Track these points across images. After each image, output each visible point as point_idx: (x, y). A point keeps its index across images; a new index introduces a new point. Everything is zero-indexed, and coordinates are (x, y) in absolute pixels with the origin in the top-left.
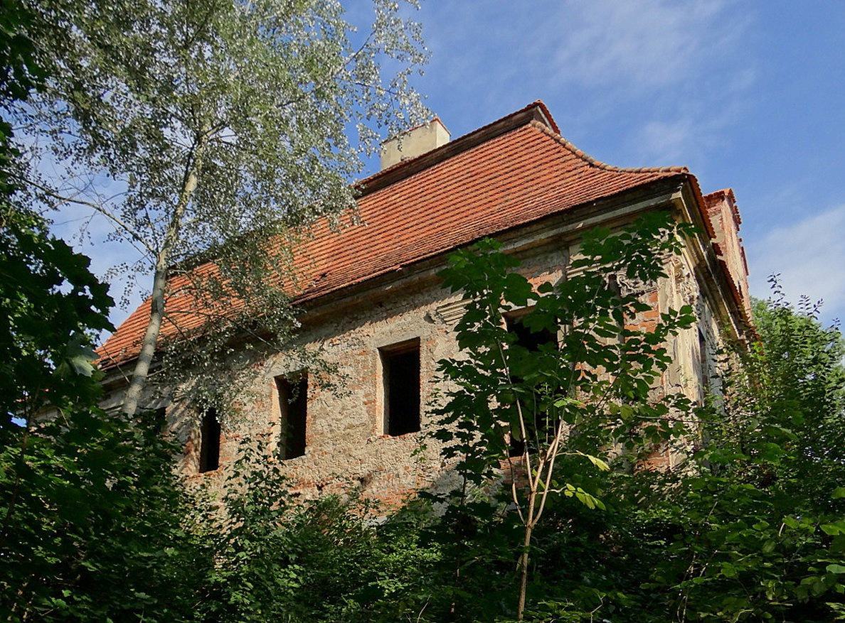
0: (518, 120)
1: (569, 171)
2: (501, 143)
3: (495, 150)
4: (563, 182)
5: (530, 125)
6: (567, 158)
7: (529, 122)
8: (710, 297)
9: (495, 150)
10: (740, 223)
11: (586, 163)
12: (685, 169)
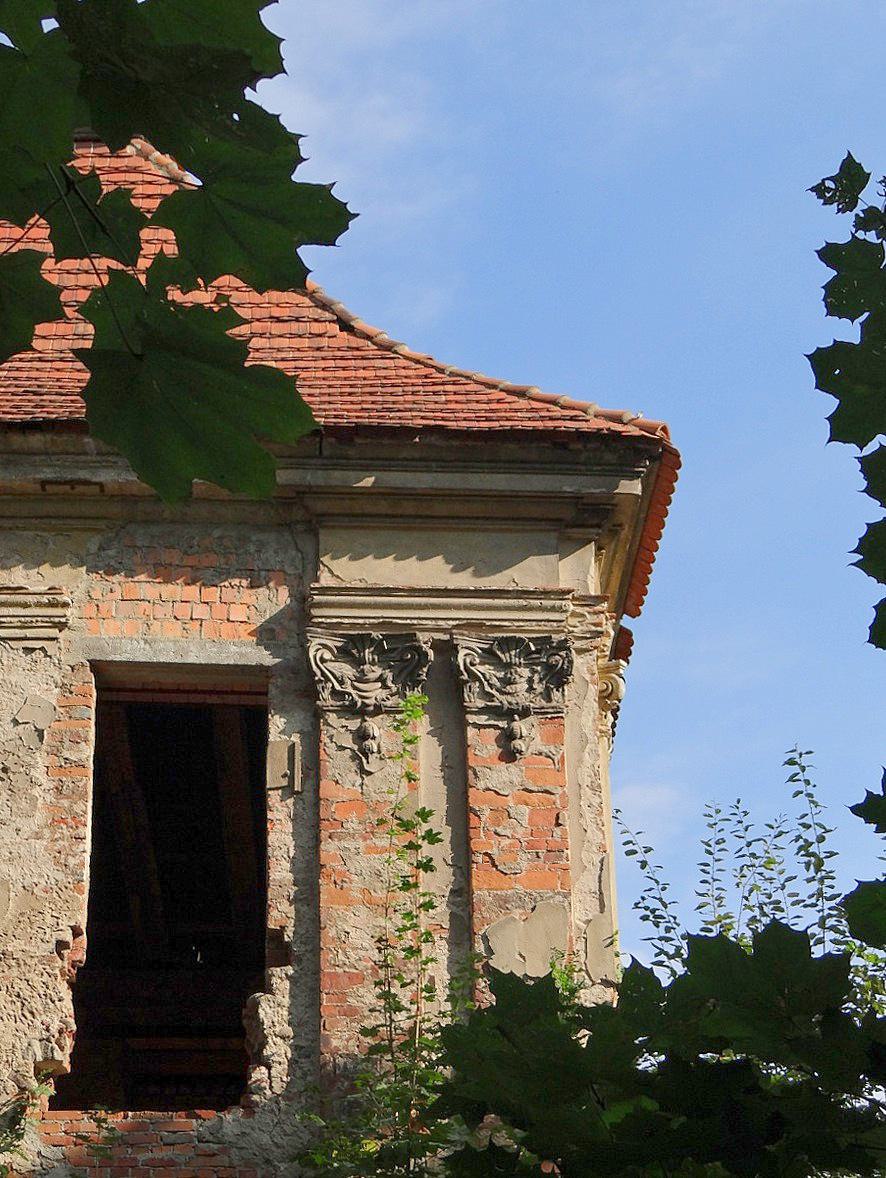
11: (327, 315)
12: (664, 429)
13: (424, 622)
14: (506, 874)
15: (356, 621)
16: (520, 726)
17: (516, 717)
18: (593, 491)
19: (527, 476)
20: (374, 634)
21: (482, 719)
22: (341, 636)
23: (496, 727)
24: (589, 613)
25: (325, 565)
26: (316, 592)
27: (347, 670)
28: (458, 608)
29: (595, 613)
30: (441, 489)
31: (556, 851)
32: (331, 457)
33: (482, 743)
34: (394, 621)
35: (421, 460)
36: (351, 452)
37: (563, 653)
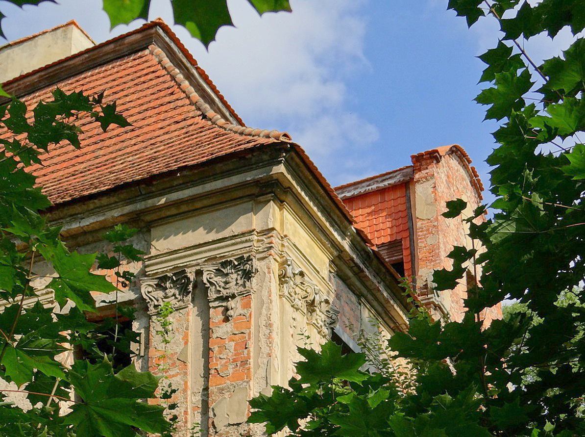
0: (132, 44)
1: (177, 122)
2: (109, 73)
3: (98, 83)
4: (167, 136)
5: (147, 52)
6: (179, 103)
7: (147, 48)
8: (370, 297)
9: (98, 83)
10: (482, 189)
11: (199, 113)
12: (285, 135)
13: (192, 262)
14: (223, 377)
15: (163, 270)
16: (231, 303)
17: (230, 299)
18: (261, 176)
19: (231, 178)
20: (169, 275)
21: (216, 304)
22: (156, 279)
23: (222, 306)
24: (266, 238)
25: (153, 246)
26: (147, 260)
27: (160, 294)
28: (205, 252)
29: (269, 238)
30: (210, 191)
31: (245, 362)
32: (145, 194)
33: (216, 315)
34: (179, 265)
35: (183, 184)
36: (154, 189)
37: (249, 263)
